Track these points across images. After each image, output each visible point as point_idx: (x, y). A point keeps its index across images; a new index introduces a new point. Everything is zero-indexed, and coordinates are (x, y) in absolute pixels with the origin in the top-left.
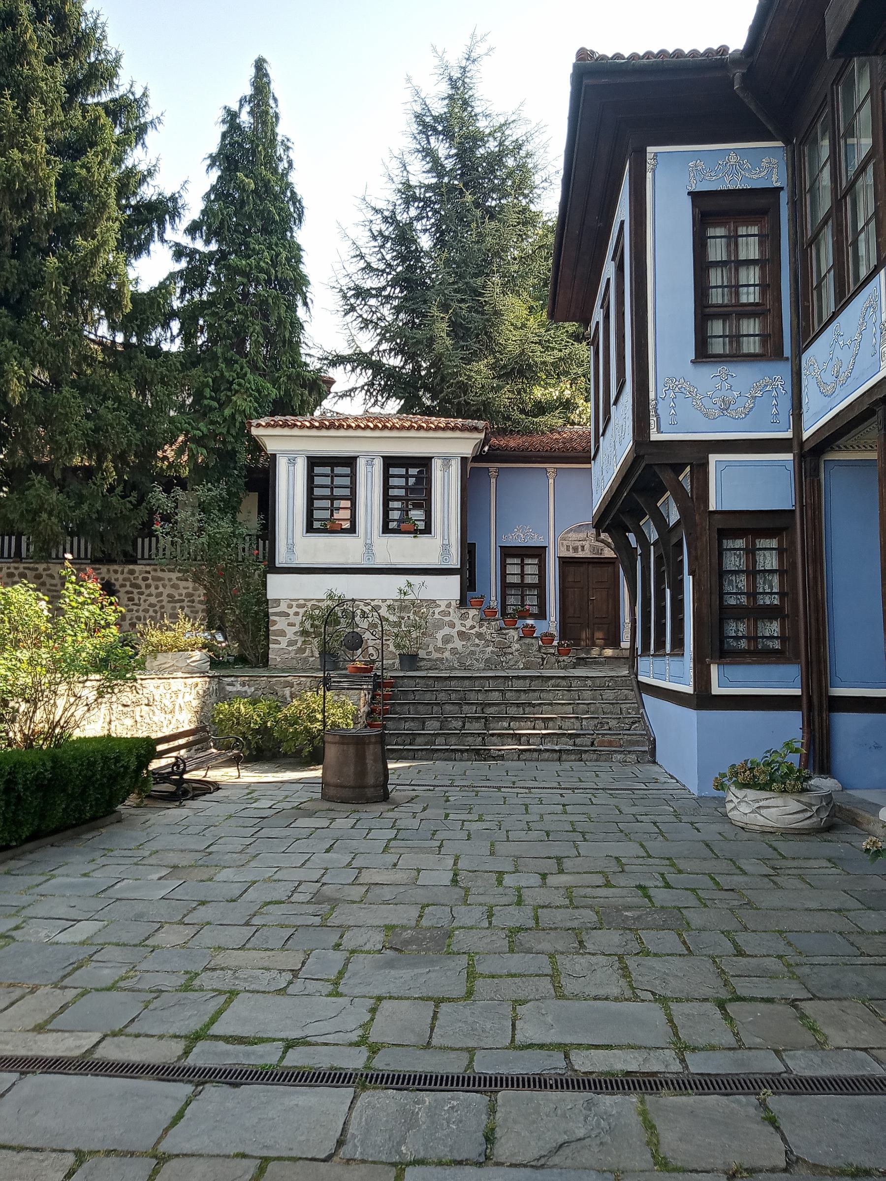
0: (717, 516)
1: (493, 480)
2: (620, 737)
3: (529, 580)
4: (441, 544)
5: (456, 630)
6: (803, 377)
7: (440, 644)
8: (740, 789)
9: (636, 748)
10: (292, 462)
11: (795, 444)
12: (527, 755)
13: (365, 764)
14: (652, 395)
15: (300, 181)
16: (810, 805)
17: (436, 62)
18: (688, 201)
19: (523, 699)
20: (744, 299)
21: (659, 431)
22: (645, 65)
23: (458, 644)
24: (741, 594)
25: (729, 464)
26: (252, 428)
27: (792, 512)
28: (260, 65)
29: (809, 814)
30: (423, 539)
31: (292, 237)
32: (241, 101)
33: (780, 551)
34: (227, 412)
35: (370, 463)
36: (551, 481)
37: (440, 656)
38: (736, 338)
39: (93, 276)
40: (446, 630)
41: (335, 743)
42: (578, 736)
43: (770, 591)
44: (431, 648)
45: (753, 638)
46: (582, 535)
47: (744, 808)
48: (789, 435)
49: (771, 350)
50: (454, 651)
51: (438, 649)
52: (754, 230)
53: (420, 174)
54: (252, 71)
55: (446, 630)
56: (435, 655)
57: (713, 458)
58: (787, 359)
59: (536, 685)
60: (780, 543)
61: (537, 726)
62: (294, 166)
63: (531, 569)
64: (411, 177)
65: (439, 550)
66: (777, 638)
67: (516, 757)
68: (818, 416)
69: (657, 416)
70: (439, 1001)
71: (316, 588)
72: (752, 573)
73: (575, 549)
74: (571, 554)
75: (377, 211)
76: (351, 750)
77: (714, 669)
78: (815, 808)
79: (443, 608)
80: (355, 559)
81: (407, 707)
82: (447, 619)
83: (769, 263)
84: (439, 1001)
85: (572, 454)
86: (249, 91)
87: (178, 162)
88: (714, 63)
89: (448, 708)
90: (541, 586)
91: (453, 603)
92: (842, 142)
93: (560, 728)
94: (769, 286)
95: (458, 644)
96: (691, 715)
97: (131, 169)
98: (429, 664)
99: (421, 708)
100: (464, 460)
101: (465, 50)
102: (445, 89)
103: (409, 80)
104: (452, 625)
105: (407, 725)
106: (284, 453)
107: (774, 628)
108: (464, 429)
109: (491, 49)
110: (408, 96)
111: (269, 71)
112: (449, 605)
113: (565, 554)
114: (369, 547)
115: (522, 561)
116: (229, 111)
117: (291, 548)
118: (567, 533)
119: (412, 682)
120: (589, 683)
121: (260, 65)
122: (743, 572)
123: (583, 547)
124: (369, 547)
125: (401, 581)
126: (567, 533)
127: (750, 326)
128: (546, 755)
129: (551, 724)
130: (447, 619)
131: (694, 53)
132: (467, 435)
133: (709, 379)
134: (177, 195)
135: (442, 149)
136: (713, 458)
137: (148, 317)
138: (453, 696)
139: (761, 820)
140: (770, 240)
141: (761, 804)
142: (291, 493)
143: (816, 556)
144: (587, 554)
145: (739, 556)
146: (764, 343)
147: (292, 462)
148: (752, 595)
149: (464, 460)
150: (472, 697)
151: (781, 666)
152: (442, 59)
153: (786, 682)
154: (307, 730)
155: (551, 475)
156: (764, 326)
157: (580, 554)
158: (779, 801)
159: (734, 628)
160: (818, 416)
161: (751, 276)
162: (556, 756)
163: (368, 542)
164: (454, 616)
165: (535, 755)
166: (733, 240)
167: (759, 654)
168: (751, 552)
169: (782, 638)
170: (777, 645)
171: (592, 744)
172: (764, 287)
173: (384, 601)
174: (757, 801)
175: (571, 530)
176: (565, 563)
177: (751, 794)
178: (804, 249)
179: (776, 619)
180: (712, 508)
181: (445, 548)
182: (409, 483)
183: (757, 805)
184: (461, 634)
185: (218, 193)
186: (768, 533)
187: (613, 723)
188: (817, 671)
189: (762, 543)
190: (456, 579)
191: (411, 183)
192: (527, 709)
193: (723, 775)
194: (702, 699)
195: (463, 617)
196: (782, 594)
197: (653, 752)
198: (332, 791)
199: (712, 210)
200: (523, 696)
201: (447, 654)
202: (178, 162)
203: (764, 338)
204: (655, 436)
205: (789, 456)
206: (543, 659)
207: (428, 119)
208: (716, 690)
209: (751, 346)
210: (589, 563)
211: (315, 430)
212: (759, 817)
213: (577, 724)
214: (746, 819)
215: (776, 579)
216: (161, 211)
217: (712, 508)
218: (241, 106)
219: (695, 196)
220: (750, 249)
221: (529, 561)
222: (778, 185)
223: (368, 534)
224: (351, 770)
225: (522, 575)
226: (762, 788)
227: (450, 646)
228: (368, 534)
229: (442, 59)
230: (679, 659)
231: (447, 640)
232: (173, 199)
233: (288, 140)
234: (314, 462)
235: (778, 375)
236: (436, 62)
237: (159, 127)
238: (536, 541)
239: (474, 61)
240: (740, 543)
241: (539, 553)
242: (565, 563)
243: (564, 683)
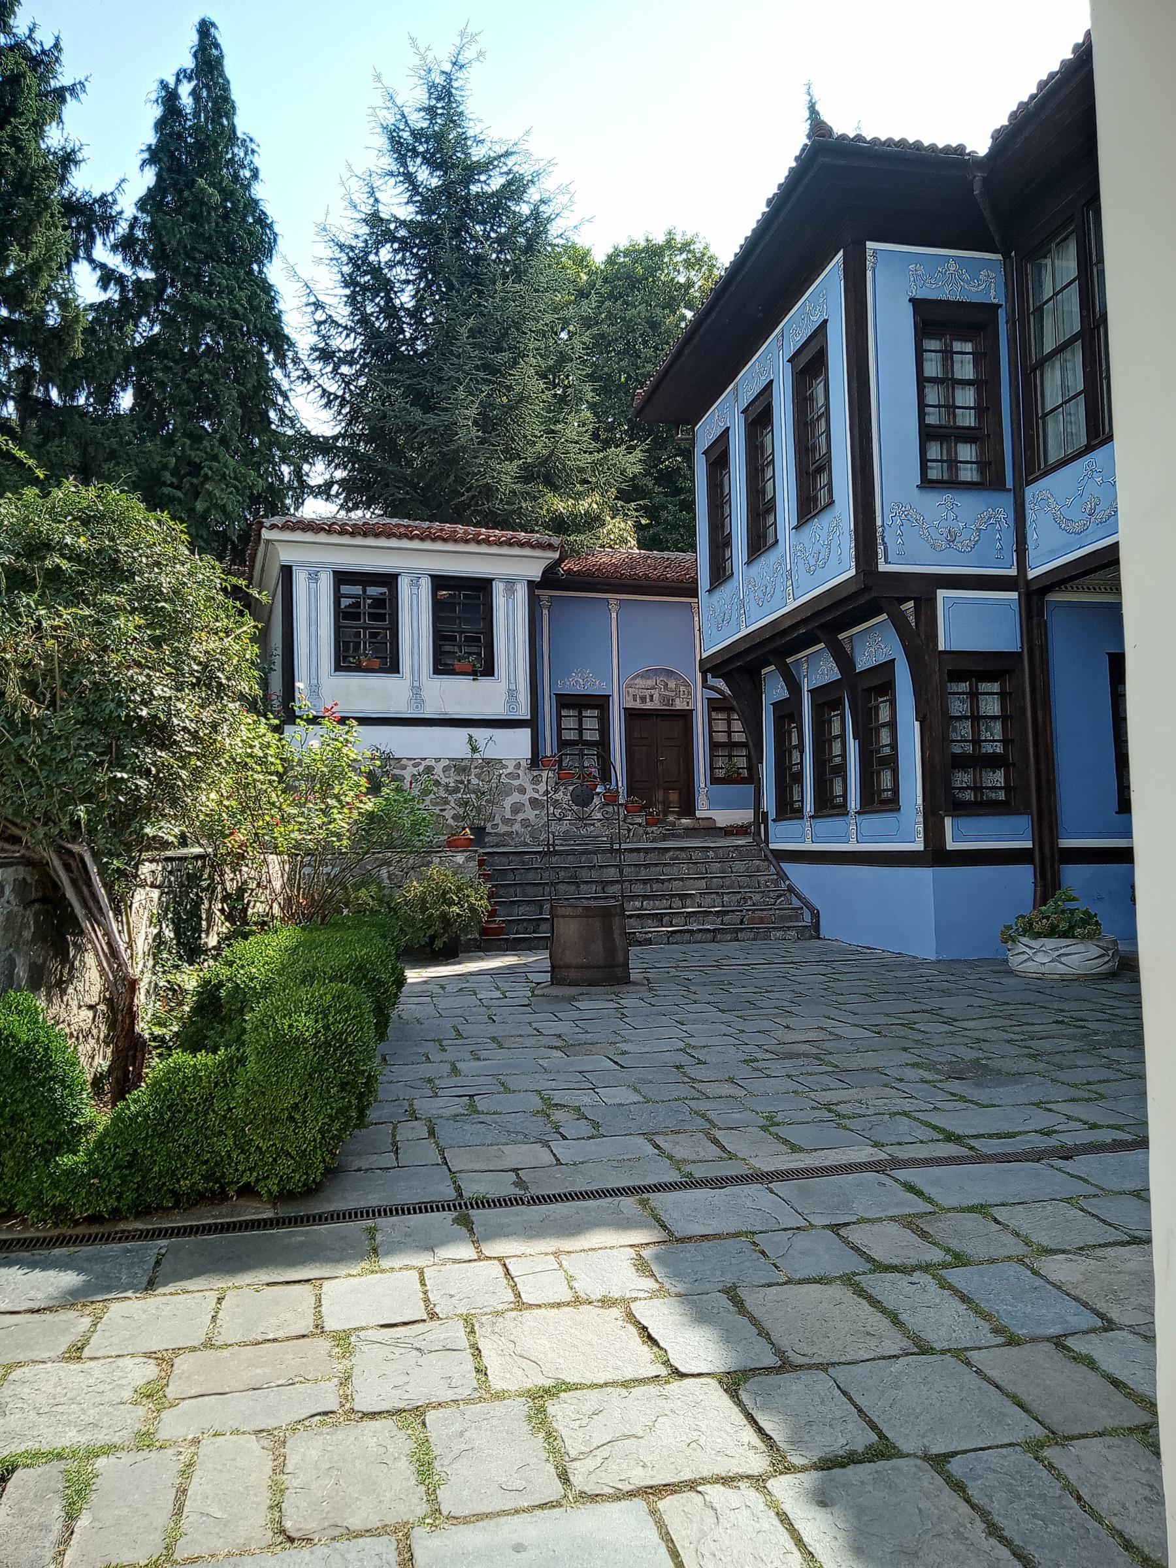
0: (946, 656)
1: (545, 612)
2: (771, 912)
3: (587, 736)
4: (502, 691)
5: (527, 796)
6: (1029, 512)
7: (508, 816)
8: (1036, 939)
9: (796, 924)
10: (314, 577)
11: (1022, 584)
12: (678, 937)
13: (612, 939)
14: (879, 522)
15: (268, 194)
16: (1106, 949)
17: (417, 61)
18: (910, 307)
19: (644, 874)
20: (961, 422)
21: (886, 562)
22: (887, 152)
23: (530, 814)
24: (966, 741)
25: (956, 602)
26: (263, 530)
27: (1017, 655)
28: (205, 29)
29: (1107, 959)
30: (484, 683)
31: (261, 272)
32: (178, 75)
33: (1003, 695)
34: (200, 506)
35: (415, 583)
36: (614, 615)
37: (508, 829)
38: (953, 463)
39: (31, 302)
40: (516, 797)
41: (576, 917)
42: (726, 913)
43: (993, 739)
44: (497, 820)
45: (977, 789)
46: (651, 683)
47: (1041, 958)
48: (1013, 572)
49: (990, 479)
50: (525, 823)
51: (506, 821)
52: (968, 347)
53: (397, 205)
54: (194, 38)
55: (516, 797)
56: (502, 829)
57: (941, 594)
58: (1010, 490)
59: (652, 858)
60: (1002, 686)
61: (674, 905)
62: (261, 176)
63: (591, 723)
64: (381, 207)
65: (505, 697)
66: (1000, 788)
67: (665, 941)
68: (1055, 553)
69: (884, 544)
70: (209, 1344)
71: (363, 744)
72: (976, 718)
73: (643, 699)
74: (638, 705)
75: (341, 247)
76: (597, 924)
77: (948, 822)
78: (1110, 953)
79: (510, 769)
80: (400, 707)
81: (512, 890)
82: (516, 783)
83: (986, 384)
84: (209, 1344)
85: (644, 582)
86: (189, 63)
87: (107, 150)
88: (950, 163)
89: (562, 887)
90: (604, 743)
91: (523, 763)
92: (1095, 270)
93: (700, 906)
94: (987, 407)
95: (530, 814)
96: (925, 874)
97: (70, 154)
98: (495, 840)
99: (529, 889)
100: (531, 583)
101: (453, 50)
102: (421, 96)
103: (378, 78)
104: (522, 791)
105: (522, 909)
106: (303, 564)
107: (997, 778)
108: (540, 546)
109: (481, 54)
110: (378, 100)
111: (220, 41)
112: (518, 766)
113: (630, 704)
114: (416, 691)
115: (580, 713)
116: (164, 85)
117: (315, 690)
118: (634, 678)
119: (504, 860)
120: (711, 854)
121: (205, 29)
122: (966, 718)
123: (652, 696)
124: (416, 691)
125: (460, 735)
126: (634, 678)
127: (966, 452)
128: (699, 936)
129: (689, 902)
130: (516, 783)
131: (933, 147)
132: (538, 553)
133: (936, 505)
134: (110, 199)
135: (428, 178)
136: (941, 594)
137: (94, 367)
138: (562, 874)
139: (1062, 969)
140: (986, 358)
141: (1061, 951)
142: (313, 628)
143: (1043, 700)
144: (656, 705)
145: (962, 701)
146: (981, 471)
147: (314, 577)
148: (976, 742)
149: (531, 583)
150: (585, 874)
151: (975, 819)
152: (424, 58)
153: (1013, 834)
154: (444, 917)
155: (613, 606)
156: (981, 453)
157: (649, 705)
158: (1080, 948)
159: (962, 779)
160: (1055, 553)
161: (966, 397)
162: (709, 936)
163: (418, 682)
164: (524, 780)
165: (687, 936)
166: (947, 355)
167: (981, 806)
168: (974, 696)
169: (1007, 788)
170: (1001, 796)
171: (742, 922)
172: (980, 410)
173: (438, 760)
174: (1056, 949)
175: (637, 676)
176: (633, 716)
177: (1050, 943)
178: (1030, 373)
179: (999, 768)
180: (941, 648)
181: (512, 694)
182: (463, 612)
183: (1057, 953)
184: (534, 802)
185: (150, 201)
186: (990, 677)
187: (756, 898)
188: (1046, 824)
189: (984, 687)
190: (525, 734)
191: (382, 215)
192: (655, 886)
193: (1009, 927)
194: (936, 855)
195: (536, 780)
196: (1005, 742)
197: (816, 926)
198: (573, 974)
199: (934, 320)
200: (643, 871)
201: (517, 827)
202: (107, 150)
203: (982, 465)
204: (883, 567)
205: (1014, 595)
206: (629, 830)
207: (406, 135)
208: (951, 845)
209: (968, 474)
210: (658, 715)
211: (347, 536)
212: (1060, 966)
213: (718, 900)
214: (1043, 969)
215: (997, 727)
216: (90, 217)
217: (941, 648)
218: (178, 81)
219: (918, 304)
220: (965, 369)
221: (588, 713)
222: (996, 301)
223: (416, 671)
224: (598, 947)
225: (580, 730)
226: (1064, 935)
227: (520, 817)
228: (416, 671)
229: (424, 58)
230: (895, 815)
231: (517, 808)
232: (102, 201)
233: (251, 140)
234: (342, 578)
235: (1001, 507)
236: (417, 61)
237: (82, 96)
238: (595, 687)
239: (461, 67)
240: (964, 687)
241: (601, 703)
242: (633, 716)
243: (683, 855)
